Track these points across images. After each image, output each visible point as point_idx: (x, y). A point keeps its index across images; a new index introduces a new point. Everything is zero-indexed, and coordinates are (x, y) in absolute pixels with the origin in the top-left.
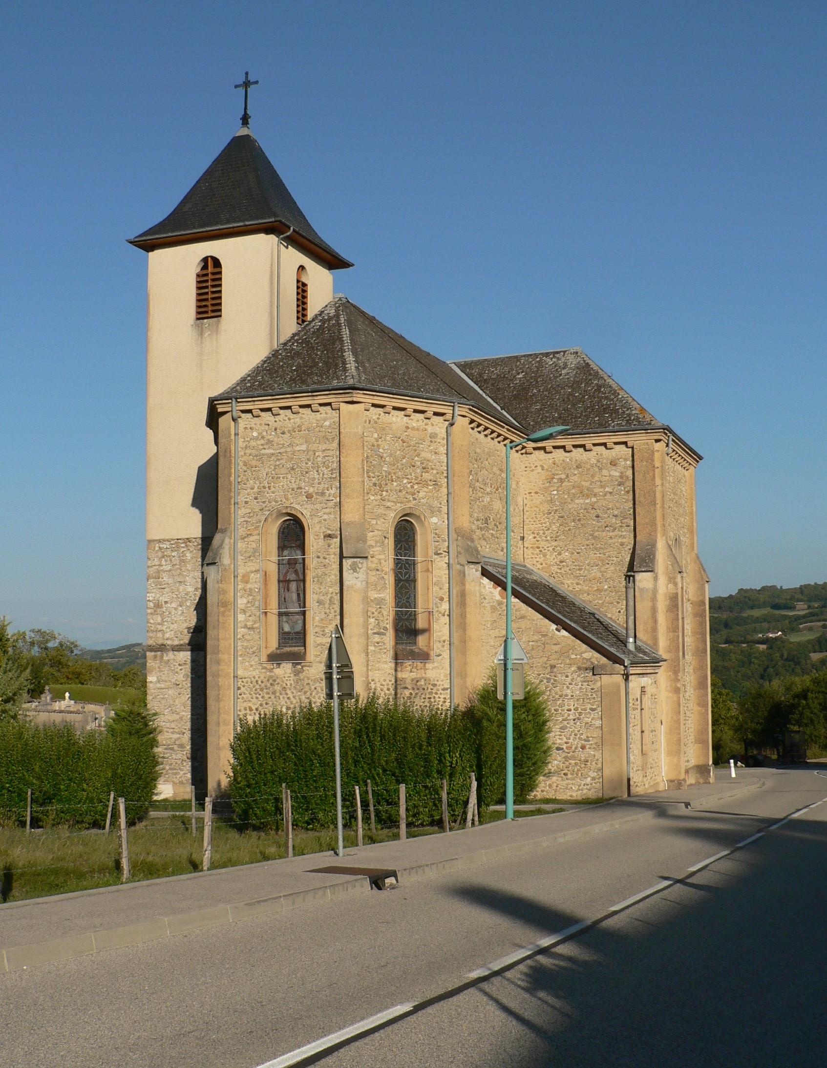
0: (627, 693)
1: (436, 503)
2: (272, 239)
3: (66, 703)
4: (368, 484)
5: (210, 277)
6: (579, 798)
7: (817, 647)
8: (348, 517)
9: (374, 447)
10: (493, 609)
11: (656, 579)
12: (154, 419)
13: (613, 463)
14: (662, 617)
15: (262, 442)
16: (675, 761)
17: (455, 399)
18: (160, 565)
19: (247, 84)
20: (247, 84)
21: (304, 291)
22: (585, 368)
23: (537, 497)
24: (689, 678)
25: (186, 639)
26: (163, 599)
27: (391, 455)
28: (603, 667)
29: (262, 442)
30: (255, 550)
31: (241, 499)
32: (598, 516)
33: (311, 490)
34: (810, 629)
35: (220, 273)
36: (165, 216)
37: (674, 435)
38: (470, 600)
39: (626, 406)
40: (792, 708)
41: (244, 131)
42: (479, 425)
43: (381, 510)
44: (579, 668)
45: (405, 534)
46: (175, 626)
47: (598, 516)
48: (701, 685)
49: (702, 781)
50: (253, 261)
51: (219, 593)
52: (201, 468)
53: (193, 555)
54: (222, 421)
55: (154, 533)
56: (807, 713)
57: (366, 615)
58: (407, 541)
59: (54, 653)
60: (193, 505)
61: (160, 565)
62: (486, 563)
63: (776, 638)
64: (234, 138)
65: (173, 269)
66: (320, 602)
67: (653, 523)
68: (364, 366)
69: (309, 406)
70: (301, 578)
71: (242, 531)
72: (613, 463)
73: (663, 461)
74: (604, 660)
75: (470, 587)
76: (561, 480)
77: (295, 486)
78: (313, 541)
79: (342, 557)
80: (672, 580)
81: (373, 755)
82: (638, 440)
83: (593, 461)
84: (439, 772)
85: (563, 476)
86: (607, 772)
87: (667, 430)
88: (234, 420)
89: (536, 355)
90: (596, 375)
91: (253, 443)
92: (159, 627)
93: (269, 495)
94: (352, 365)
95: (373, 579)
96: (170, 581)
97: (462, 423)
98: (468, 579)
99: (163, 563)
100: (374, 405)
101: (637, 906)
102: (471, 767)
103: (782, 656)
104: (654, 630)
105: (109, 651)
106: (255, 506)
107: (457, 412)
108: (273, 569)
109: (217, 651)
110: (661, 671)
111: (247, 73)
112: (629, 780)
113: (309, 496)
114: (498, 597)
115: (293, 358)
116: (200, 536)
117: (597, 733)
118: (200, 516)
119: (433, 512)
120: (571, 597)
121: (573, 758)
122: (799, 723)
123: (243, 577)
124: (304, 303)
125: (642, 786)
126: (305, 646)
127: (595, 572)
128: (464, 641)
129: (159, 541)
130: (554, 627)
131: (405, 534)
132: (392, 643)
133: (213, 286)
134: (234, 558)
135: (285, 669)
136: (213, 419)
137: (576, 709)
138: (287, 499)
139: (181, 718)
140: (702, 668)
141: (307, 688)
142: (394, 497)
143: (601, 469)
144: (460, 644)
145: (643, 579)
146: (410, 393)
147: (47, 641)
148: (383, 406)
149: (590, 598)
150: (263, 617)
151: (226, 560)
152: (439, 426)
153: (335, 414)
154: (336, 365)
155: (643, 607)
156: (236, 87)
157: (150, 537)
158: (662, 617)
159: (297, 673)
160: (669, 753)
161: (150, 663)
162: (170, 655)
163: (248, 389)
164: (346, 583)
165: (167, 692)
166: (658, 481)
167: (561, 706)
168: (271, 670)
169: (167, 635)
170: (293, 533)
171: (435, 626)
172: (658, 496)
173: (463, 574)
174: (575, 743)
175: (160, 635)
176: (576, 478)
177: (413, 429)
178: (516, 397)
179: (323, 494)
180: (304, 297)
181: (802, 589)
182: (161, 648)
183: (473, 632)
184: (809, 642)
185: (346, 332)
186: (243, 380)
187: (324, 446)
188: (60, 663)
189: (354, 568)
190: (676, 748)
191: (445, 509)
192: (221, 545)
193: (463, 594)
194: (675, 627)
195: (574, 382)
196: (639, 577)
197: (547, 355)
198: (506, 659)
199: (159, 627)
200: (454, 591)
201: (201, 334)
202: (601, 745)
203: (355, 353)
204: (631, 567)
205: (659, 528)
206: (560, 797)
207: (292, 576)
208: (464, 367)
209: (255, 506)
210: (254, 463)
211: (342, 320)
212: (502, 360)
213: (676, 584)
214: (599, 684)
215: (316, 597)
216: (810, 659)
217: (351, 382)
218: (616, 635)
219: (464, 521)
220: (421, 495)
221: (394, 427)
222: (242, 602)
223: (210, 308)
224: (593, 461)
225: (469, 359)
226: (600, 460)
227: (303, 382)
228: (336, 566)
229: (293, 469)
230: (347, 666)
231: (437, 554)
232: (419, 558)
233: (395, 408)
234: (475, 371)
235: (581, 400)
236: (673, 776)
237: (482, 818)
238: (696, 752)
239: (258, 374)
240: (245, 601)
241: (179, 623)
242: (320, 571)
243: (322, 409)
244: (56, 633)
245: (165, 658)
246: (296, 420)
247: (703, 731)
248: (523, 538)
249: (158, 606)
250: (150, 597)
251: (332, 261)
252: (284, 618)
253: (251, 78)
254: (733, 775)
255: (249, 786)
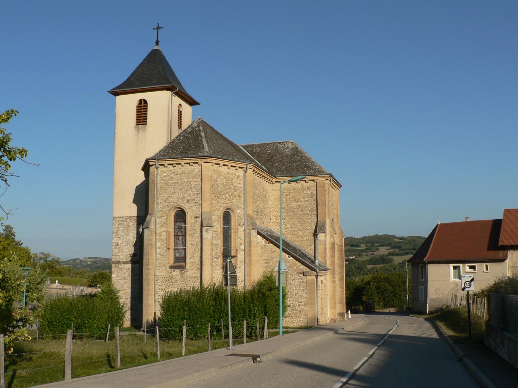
0: (317, 283)
1: (239, 204)
2: (169, 93)
3: (57, 285)
4: (213, 196)
5: (142, 107)
6: (298, 326)
7: (370, 263)
8: (204, 210)
9: (216, 181)
10: (262, 248)
11: (326, 236)
12: (117, 166)
13: (308, 188)
14: (328, 252)
15: (168, 178)
16: (333, 311)
17: (247, 161)
18: (118, 228)
19: (158, 28)
20: (158, 28)
21: (181, 114)
22: (296, 149)
23: (272, 200)
24: (337, 277)
25: (129, 259)
26: (119, 242)
27: (222, 184)
28: (307, 272)
29: (168, 178)
30: (165, 223)
31: (159, 201)
32: (302, 210)
33: (189, 198)
34: (367, 255)
35: (147, 106)
36: (123, 81)
37: (333, 177)
38: (253, 244)
39: (314, 165)
40: (364, 288)
41: (156, 48)
42: (256, 172)
43: (218, 207)
44: (298, 273)
45: (227, 217)
46: (124, 253)
47: (302, 210)
48: (341, 280)
49: (341, 319)
50: (160, 101)
51: (149, 240)
52: (137, 188)
53: (133, 224)
54: (151, 169)
55: (116, 214)
56: (370, 291)
57: (212, 250)
58: (227, 220)
59: (50, 263)
60: (133, 202)
61: (118, 228)
62: (259, 229)
63: (353, 259)
64: (153, 50)
65: (127, 103)
66: (192, 245)
67: (325, 213)
68: (211, 148)
69: (189, 163)
70: (184, 234)
71: (159, 215)
72: (308, 188)
73: (329, 188)
74: (308, 270)
75: (253, 239)
76: (287, 195)
77: (182, 196)
78: (189, 219)
79: (202, 226)
80: (332, 236)
81: (221, 308)
82: (319, 179)
83: (300, 187)
84: (249, 316)
85: (288, 193)
86: (309, 316)
87: (330, 175)
88: (156, 168)
89: (275, 143)
90: (301, 152)
91: (164, 178)
92: (118, 254)
93: (171, 200)
94: (206, 147)
95: (214, 235)
96: (123, 234)
97: (250, 171)
98: (252, 235)
99: (120, 226)
100: (216, 164)
101: (362, 367)
102: (262, 313)
103: (355, 267)
104: (325, 257)
105: (65, 262)
106: (165, 204)
107: (248, 167)
108: (172, 230)
109: (148, 264)
110: (328, 274)
111: (158, 24)
112: (318, 319)
113: (188, 201)
114: (264, 243)
115: (181, 143)
116: (136, 215)
117: (305, 300)
118: (136, 207)
119: (238, 208)
120: (291, 243)
121: (295, 310)
122: (366, 295)
123: (159, 233)
124: (181, 119)
125: (322, 322)
126: (185, 263)
127: (301, 233)
128: (250, 261)
129: (118, 217)
130: (287, 256)
131: (227, 217)
132: (222, 262)
133: (144, 111)
134: (156, 226)
135: (177, 273)
136: (146, 168)
137: (296, 290)
138: (179, 202)
139: (126, 293)
140: (342, 272)
141: (186, 281)
142: (223, 202)
143: (303, 191)
144: (248, 263)
145: (321, 236)
146: (230, 159)
147: (47, 258)
148: (219, 164)
149: (298, 243)
150: (167, 250)
151: (152, 226)
152: (241, 172)
153: (200, 167)
154: (200, 147)
155: (320, 248)
156: (154, 29)
157: (114, 216)
158: (328, 252)
159: (182, 274)
160: (331, 308)
161: (113, 269)
162: (122, 266)
163: (162, 155)
164: (204, 237)
165: (121, 281)
166: (327, 196)
167: (290, 288)
168: (171, 273)
169: (121, 257)
170: (181, 216)
171: (239, 255)
172: (327, 202)
173: (250, 234)
174: (296, 303)
175: (118, 257)
176: (293, 194)
177: (231, 174)
178: (267, 160)
179: (194, 200)
180: (181, 117)
181: (363, 238)
182: (118, 263)
183: (254, 258)
184: (366, 260)
185: (203, 133)
186: (160, 152)
187: (195, 180)
188: (52, 267)
189: (207, 231)
190: (333, 307)
191: (243, 207)
192: (150, 220)
193: (250, 242)
194: (333, 256)
195: (292, 155)
196: (320, 235)
197: (280, 143)
198: (279, 270)
199: (118, 254)
200: (246, 240)
201: (138, 131)
202: (307, 304)
203: (207, 142)
204: (316, 231)
205: (327, 215)
206: (291, 326)
207: (180, 234)
208: (245, 147)
209: (165, 204)
210: (165, 186)
211: (201, 128)
212: (261, 144)
213: (334, 238)
214: (306, 279)
215: (190, 242)
216: (367, 268)
217: (206, 154)
218: (310, 259)
219: (250, 211)
220: (234, 201)
221: (223, 173)
222: (158, 244)
223: (142, 121)
224: (300, 187)
225: (247, 144)
226: (305, 187)
227: (186, 153)
228: (199, 230)
229: (181, 189)
230: (234, 273)
231: (239, 225)
232: (232, 227)
233: (224, 165)
234: (250, 149)
235: (295, 162)
236: (332, 317)
237: (271, 335)
238: (340, 307)
239: (166, 150)
240: (160, 244)
241: (126, 251)
242: (192, 232)
243: (194, 165)
244: (51, 254)
245: (120, 267)
246: (183, 169)
247: (342, 299)
248: (271, 219)
249: (117, 245)
250: (114, 241)
251: (192, 102)
252: (176, 251)
253: (160, 26)
254: (350, 317)
255: (169, 321)
